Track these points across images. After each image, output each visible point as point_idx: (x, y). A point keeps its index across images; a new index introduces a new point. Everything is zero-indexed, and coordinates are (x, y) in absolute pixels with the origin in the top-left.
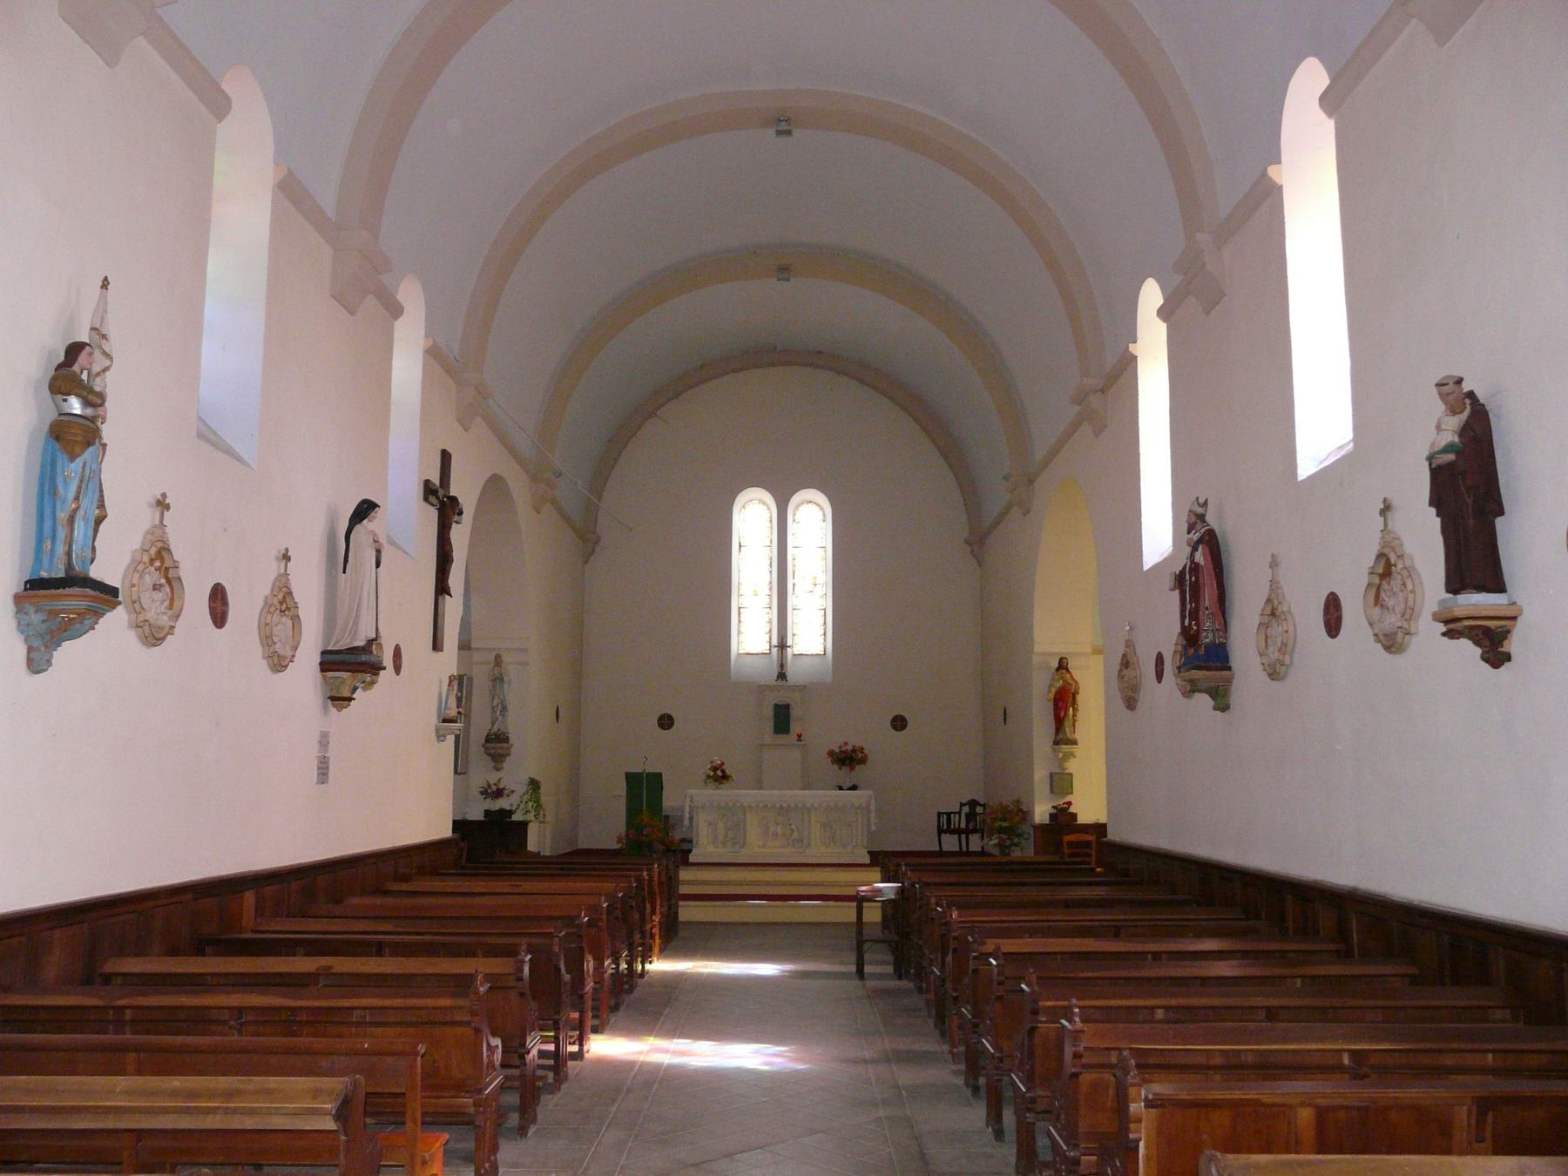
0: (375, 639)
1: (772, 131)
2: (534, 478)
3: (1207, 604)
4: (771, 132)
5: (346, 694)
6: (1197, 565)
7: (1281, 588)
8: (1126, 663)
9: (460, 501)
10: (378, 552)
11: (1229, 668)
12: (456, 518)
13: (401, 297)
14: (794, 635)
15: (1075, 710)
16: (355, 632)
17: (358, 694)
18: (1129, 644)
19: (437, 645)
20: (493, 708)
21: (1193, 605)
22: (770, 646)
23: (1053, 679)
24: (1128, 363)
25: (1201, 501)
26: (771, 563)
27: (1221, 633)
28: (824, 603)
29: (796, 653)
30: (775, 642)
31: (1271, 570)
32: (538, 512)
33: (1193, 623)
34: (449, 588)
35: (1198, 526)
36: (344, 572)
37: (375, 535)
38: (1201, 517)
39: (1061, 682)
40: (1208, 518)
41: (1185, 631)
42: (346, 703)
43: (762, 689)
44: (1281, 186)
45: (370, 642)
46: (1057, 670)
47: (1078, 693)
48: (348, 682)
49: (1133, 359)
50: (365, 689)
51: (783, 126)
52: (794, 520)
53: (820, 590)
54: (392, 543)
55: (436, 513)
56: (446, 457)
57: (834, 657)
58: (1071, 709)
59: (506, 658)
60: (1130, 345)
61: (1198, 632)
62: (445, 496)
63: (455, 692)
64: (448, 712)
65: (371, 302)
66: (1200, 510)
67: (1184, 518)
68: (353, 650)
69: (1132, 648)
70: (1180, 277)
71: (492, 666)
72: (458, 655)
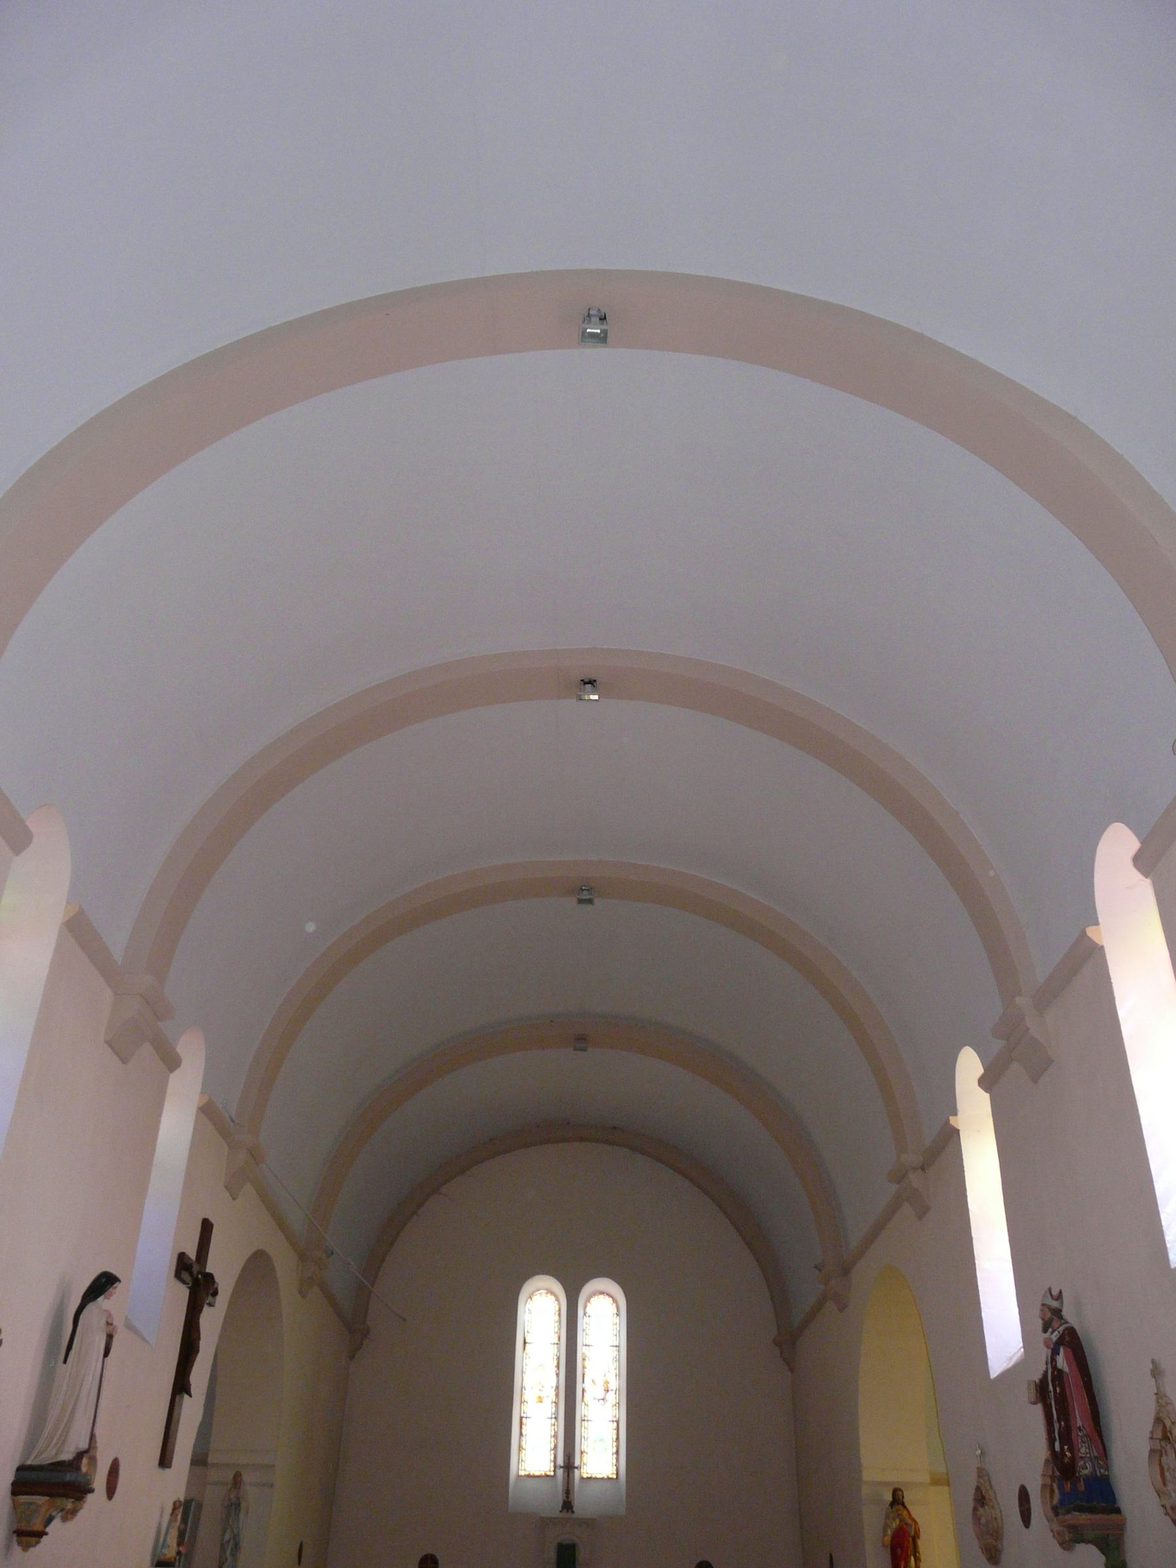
0: (86, 1452)
1: (574, 900)
2: (302, 1257)
3: (1079, 1423)
4: (570, 902)
5: (38, 1527)
6: (1061, 1372)
7: (1171, 1404)
8: (981, 1499)
9: (216, 1278)
10: (110, 1337)
11: (1118, 1511)
12: (210, 1299)
13: (179, 1049)
14: (582, 1453)
15: (917, 1560)
16: (64, 1441)
17: (55, 1527)
18: (981, 1473)
19: (165, 1461)
20: (222, 1545)
21: (1062, 1423)
22: (555, 1467)
23: (887, 1517)
24: (949, 1140)
25: (1055, 1293)
26: (558, 1363)
27: (1101, 1463)
28: (615, 1412)
29: (585, 1476)
30: (560, 1462)
31: (1153, 1379)
32: (304, 1297)
33: (1066, 1447)
34: (190, 1385)
35: (1055, 1324)
36: (65, 1362)
37: (110, 1316)
38: (1057, 1313)
39: (898, 1521)
40: (1065, 1313)
41: (1056, 1458)
42: (33, 1540)
43: (545, 1523)
44: (1102, 947)
45: (80, 1455)
46: (892, 1504)
47: (919, 1537)
48: (43, 1510)
49: (956, 1132)
50: (65, 1519)
51: (586, 896)
52: (585, 1314)
53: (612, 1398)
54: (130, 1327)
55: (187, 1292)
56: (207, 1227)
57: (627, 1482)
58: (912, 1558)
59: (247, 1478)
60: (951, 1118)
61: (1073, 1459)
62: (199, 1272)
63: (178, 1524)
64: (165, 1551)
65: (146, 1051)
66: (1055, 1304)
67: (1036, 1311)
68: (59, 1466)
69: (986, 1478)
70: (1002, 1043)
71: (229, 1487)
72: (190, 1469)
